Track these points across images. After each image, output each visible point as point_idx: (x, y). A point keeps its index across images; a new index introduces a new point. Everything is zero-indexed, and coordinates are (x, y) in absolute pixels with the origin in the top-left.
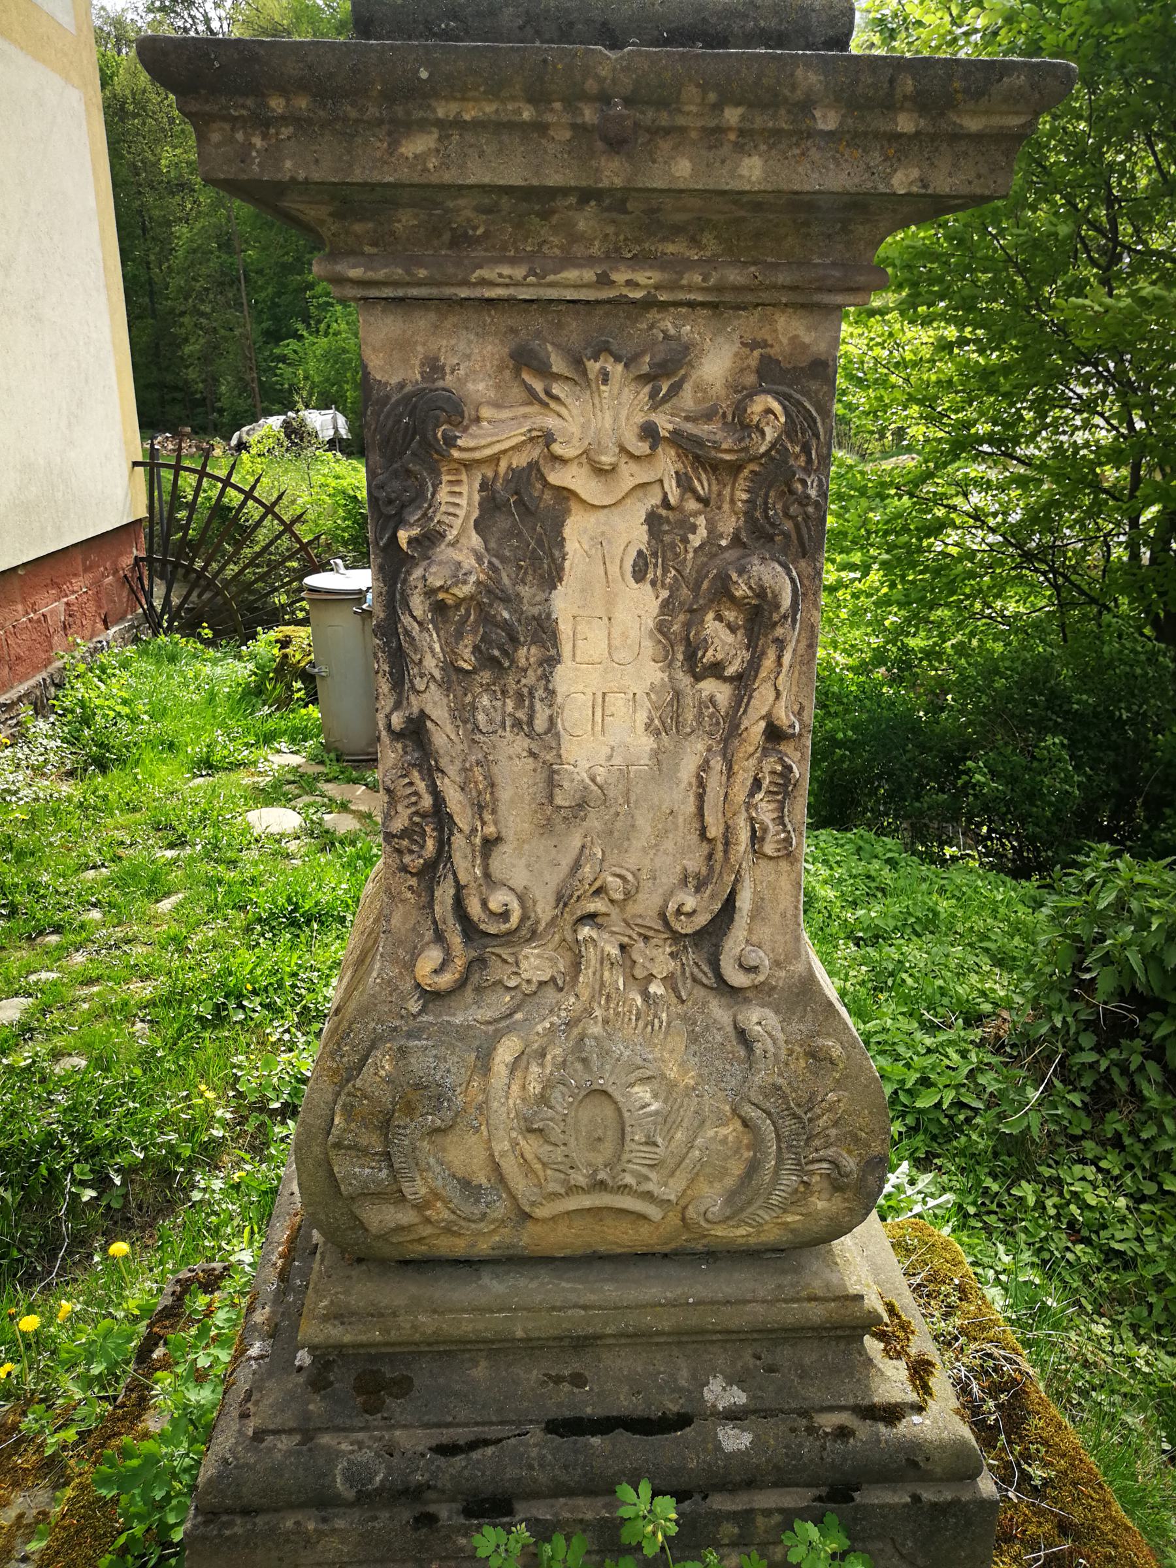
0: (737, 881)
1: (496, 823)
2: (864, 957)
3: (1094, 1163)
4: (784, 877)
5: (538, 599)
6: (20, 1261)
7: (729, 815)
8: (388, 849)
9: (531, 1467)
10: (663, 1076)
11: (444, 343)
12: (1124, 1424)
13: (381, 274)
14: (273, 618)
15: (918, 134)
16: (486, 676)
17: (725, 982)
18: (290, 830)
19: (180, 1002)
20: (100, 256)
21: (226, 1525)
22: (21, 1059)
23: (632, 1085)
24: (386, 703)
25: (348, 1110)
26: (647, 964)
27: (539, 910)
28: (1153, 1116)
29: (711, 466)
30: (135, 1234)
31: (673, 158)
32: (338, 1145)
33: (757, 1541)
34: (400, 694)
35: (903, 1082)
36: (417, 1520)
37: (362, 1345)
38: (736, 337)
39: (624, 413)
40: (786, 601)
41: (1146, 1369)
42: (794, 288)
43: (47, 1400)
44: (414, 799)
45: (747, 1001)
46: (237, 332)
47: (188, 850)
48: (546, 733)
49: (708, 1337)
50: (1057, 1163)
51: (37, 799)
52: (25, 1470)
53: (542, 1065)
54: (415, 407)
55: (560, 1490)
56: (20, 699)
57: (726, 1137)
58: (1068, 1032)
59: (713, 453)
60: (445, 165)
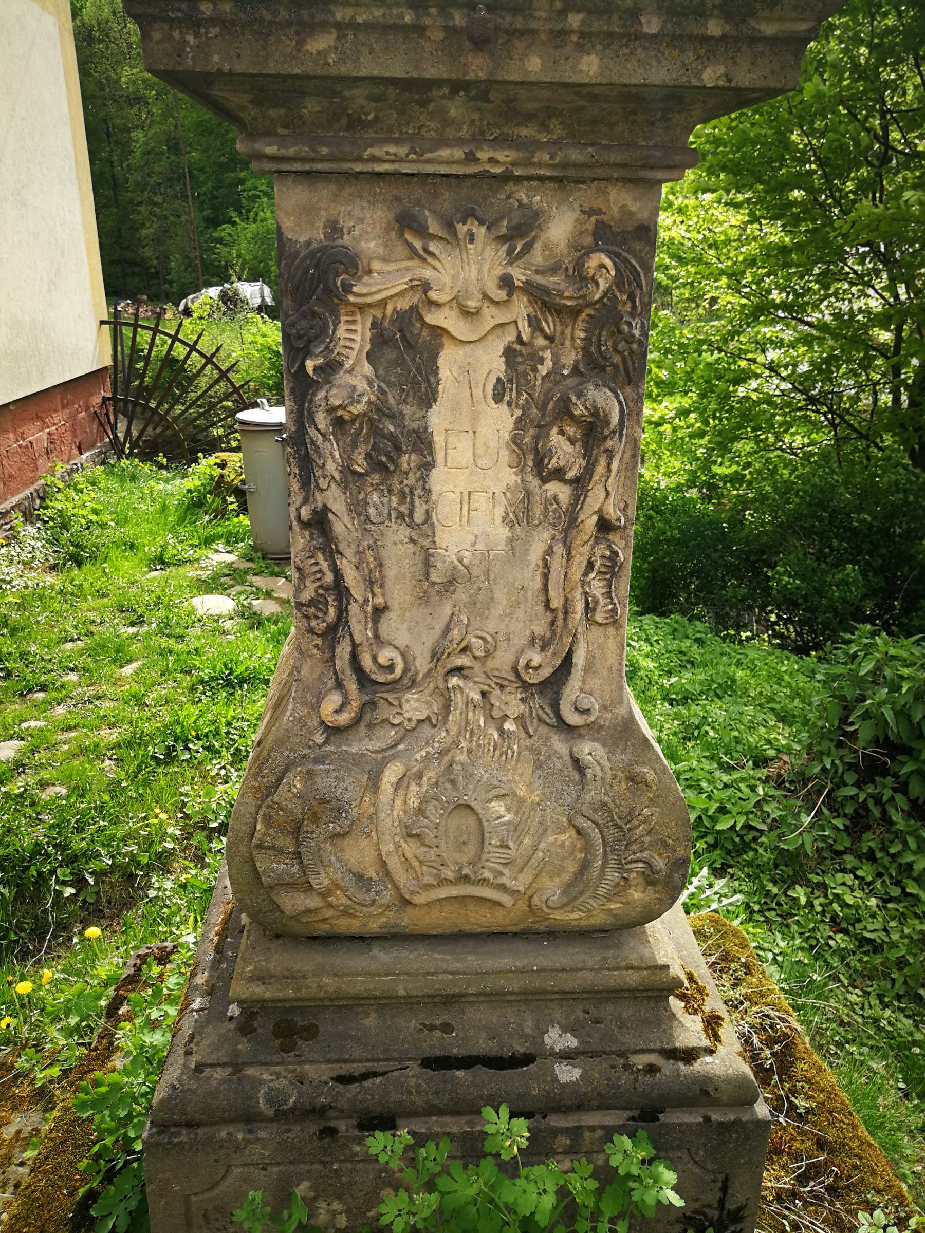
0: (573, 642)
1: (384, 595)
2: (676, 714)
3: (852, 872)
4: (611, 640)
5: (417, 415)
6: (16, 941)
7: (568, 590)
8: (299, 615)
9: (410, 1093)
10: (515, 794)
11: (343, 209)
12: (870, 1069)
13: (291, 151)
14: (211, 447)
15: (724, 36)
16: (375, 478)
17: (564, 722)
18: (225, 613)
19: (140, 744)
20: (72, 153)
21: (174, 1135)
22: (16, 787)
23: (490, 801)
24: (297, 499)
25: (267, 819)
26: (503, 707)
27: (418, 664)
28: (900, 836)
29: (556, 310)
30: (105, 923)
31: (526, 55)
32: (259, 846)
33: (585, 1150)
34: (308, 492)
35: (706, 810)
36: (321, 1132)
37: (278, 1000)
38: (576, 206)
39: (486, 267)
40: (615, 419)
41: (889, 1028)
42: (623, 166)
43: (38, 1047)
44: (319, 576)
45: (581, 736)
46: (183, 219)
47: (146, 628)
48: (423, 524)
49: (548, 996)
50: (823, 872)
51: (26, 587)
52: (21, 1097)
53: (419, 785)
54: (319, 260)
55: (432, 1111)
56: (12, 508)
57: (563, 842)
58: (836, 772)
59: (558, 300)
60: (342, 60)
